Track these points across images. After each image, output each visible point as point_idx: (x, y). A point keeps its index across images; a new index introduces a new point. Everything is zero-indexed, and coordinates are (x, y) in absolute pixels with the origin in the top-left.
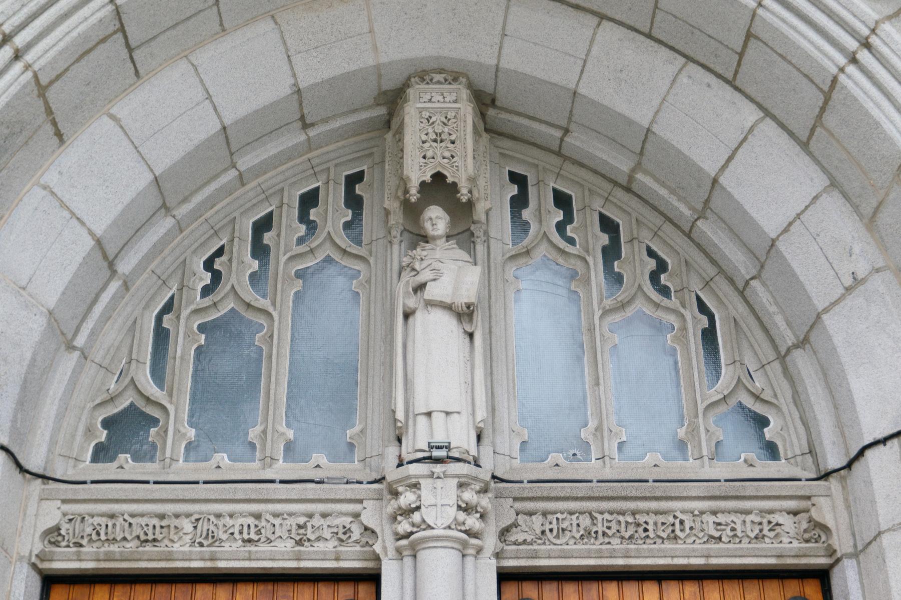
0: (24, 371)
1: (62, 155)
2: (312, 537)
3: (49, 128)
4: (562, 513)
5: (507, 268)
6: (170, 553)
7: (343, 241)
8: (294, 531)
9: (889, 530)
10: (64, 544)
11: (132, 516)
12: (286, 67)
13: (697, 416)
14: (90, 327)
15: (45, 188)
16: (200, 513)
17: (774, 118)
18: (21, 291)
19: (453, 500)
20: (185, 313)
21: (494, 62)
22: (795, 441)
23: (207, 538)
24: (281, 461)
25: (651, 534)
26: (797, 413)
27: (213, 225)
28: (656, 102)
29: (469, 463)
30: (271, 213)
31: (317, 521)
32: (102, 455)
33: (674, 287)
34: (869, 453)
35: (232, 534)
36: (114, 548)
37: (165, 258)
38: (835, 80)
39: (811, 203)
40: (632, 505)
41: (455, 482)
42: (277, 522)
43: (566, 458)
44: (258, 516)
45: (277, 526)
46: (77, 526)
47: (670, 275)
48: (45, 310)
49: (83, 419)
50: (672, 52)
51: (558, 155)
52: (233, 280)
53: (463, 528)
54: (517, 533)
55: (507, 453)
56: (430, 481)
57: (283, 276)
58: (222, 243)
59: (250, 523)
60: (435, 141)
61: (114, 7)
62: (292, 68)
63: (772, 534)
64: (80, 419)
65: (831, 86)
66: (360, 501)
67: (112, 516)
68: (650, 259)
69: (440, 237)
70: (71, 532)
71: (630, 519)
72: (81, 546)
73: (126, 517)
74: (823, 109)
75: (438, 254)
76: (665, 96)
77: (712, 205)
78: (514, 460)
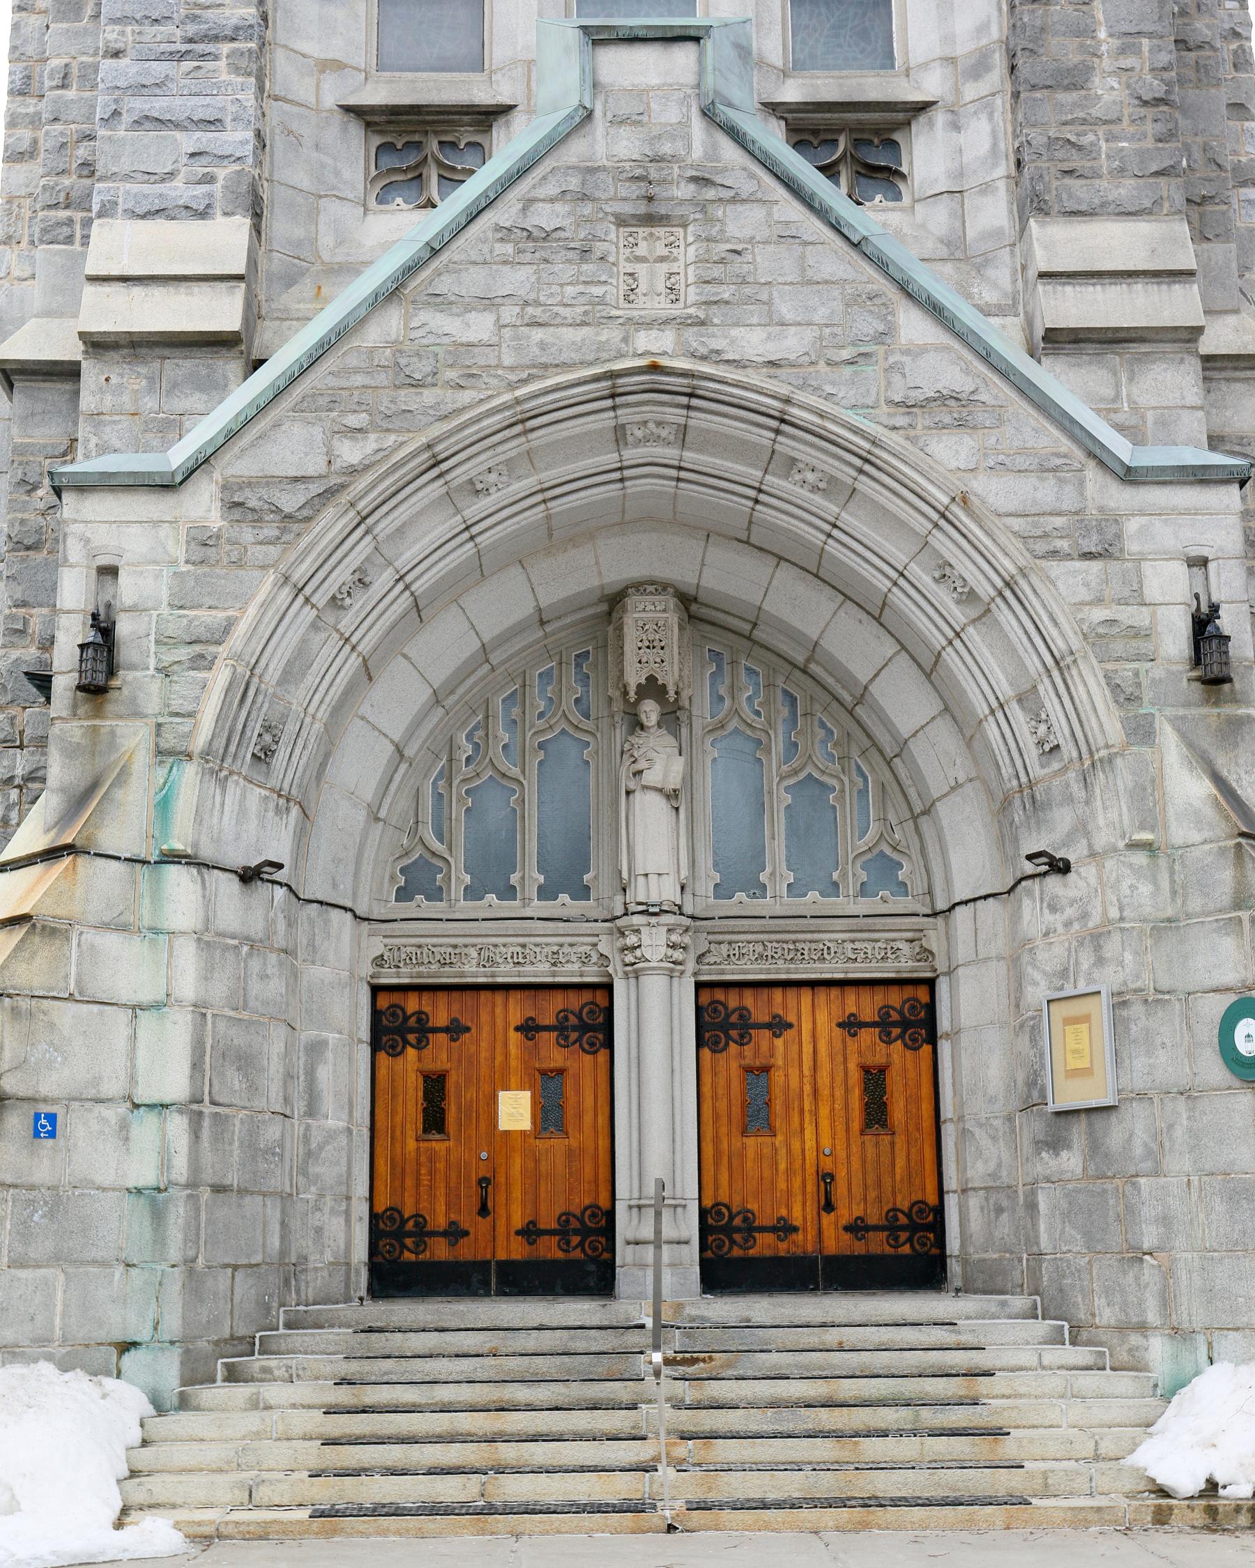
7: (576, 717)
11: (434, 946)
15: (363, 718)
17: (907, 651)
19: (663, 941)
28: (823, 625)
31: (566, 949)
34: (957, 908)
36: (422, 969)
38: (939, 653)
40: (793, 937)
41: (665, 928)
42: (538, 950)
44: (524, 946)
52: (491, 754)
60: (648, 647)
67: (420, 947)
71: (791, 947)
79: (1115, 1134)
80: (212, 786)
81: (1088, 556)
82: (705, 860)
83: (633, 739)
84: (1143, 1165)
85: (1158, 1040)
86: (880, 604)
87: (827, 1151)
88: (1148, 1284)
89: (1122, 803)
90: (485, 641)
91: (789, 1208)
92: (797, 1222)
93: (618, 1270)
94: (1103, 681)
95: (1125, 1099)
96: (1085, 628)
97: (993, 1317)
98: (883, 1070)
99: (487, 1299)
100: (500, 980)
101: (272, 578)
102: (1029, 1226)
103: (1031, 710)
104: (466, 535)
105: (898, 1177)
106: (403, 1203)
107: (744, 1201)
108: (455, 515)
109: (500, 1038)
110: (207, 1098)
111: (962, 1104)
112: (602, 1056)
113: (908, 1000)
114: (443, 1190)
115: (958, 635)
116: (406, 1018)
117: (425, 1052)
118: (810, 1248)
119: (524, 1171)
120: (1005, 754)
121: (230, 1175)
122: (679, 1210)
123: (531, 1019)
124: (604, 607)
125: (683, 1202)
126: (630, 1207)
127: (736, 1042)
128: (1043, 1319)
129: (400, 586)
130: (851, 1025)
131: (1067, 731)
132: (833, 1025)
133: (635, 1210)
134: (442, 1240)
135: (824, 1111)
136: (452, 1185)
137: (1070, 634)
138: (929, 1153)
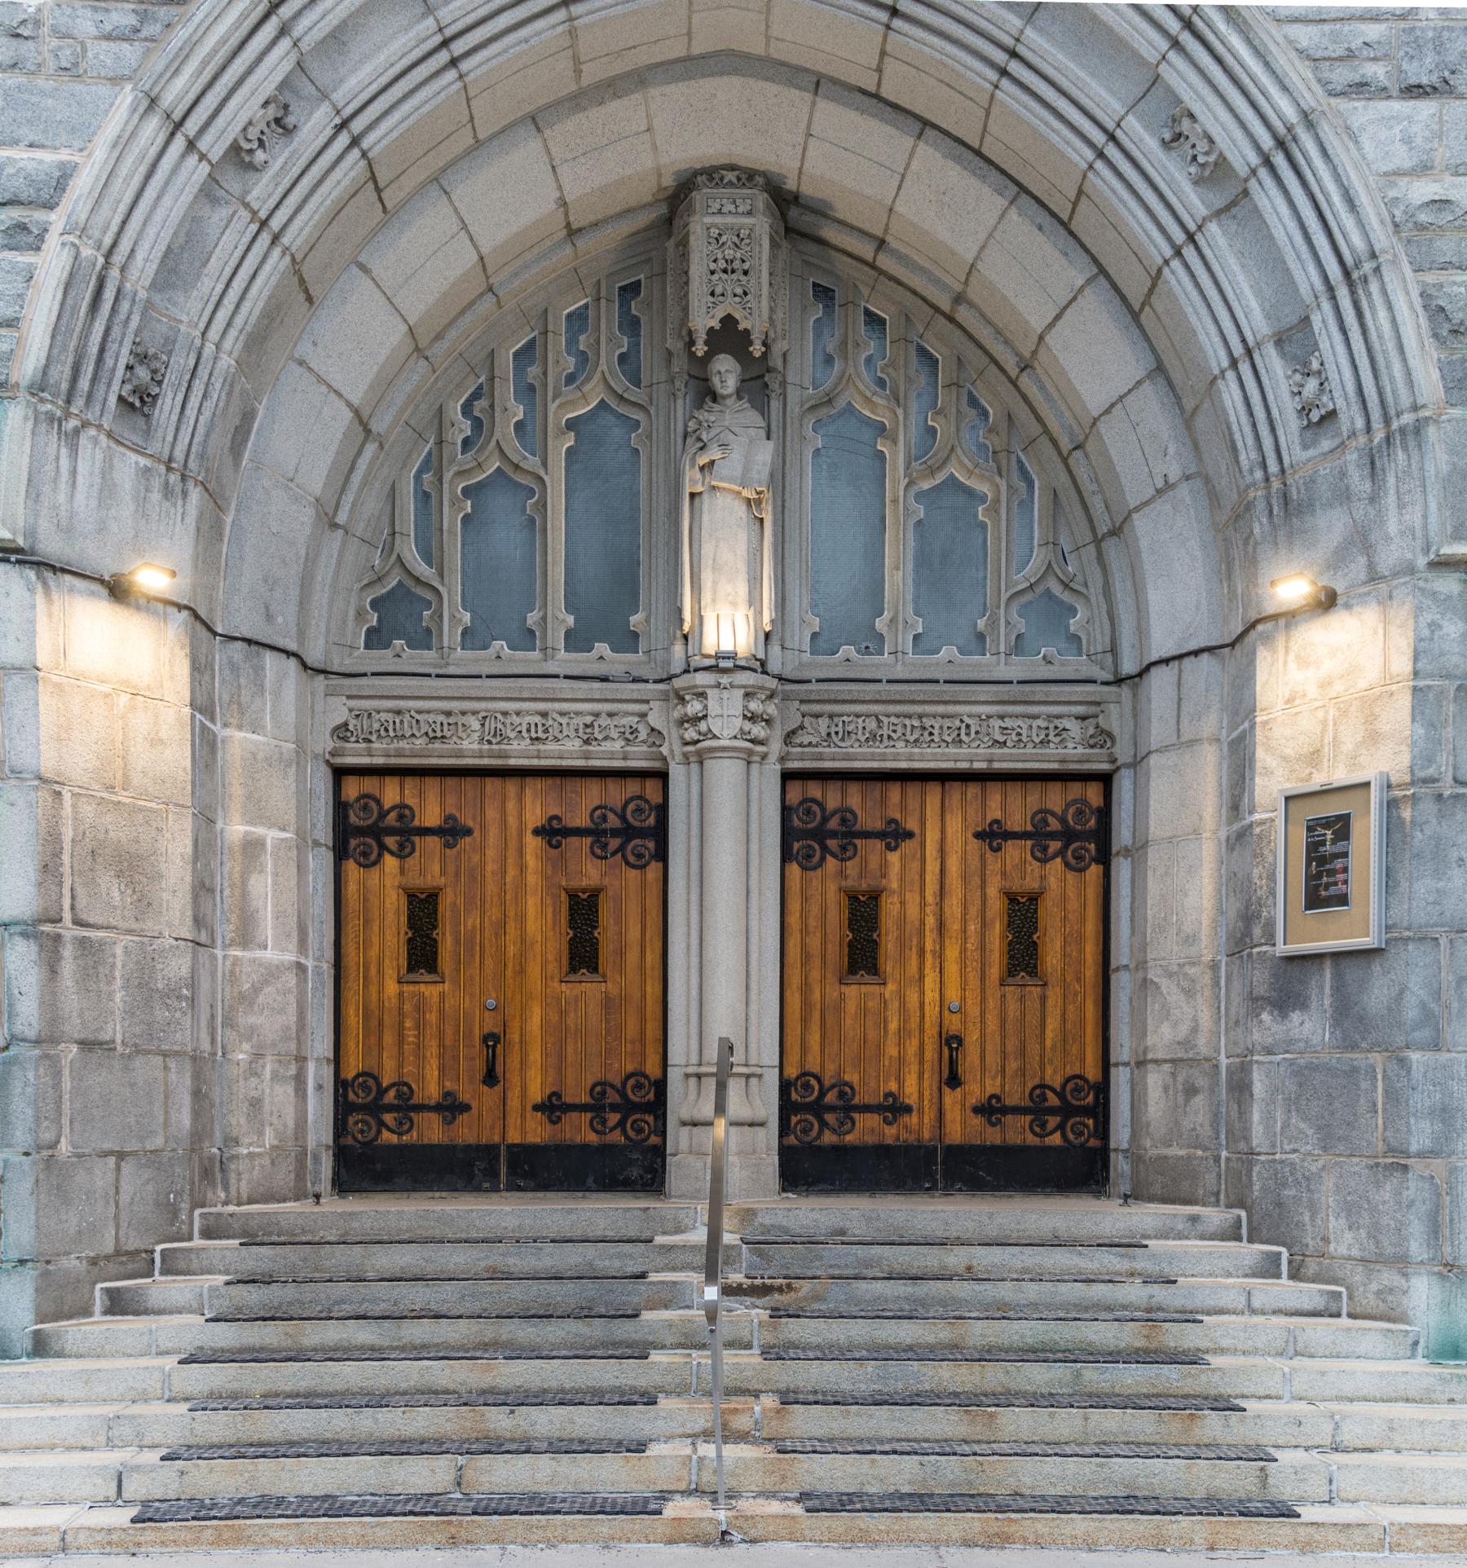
2: (600, 737)
3: (302, 297)
5: (806, 420)
6: (461, 750)
7: (620, 383)
11: (419, 712)
12: (550, 180)
13: (998, 607)
19: (739, 711)
22: (1099, 636)
23: (495, 735)
28: (982, 236)
31: (604, 721)
34: (1154, 671)
36: (403, 744)
38: (1160, 271)
40: (919, 709)
41: (742, 691)
42: (564, 721)
44: (544, 715)
49: (352, 600)
52: (497, 435)
55: (796, 646)
56: (716, 691)
60: (725, 271)
62: (557, 180)
63: (1058, 739)
66: (647, 702)
67: (399, 712)
69: (730, 396)
71: (916, 723)
72: (370, 741)
75: (728, 419)
79: (1377, 993)
80: (51, 442)
81: (1415, 91)
82: (798, 600)
83: (702, 415)
84: (1417, 1034)
85: (1454, 854)
86: (1072, 195)
87: (955, 1005)
88: (1413, 1202)
89: (1430, 498)
91: (900, 1081)
92: (911, 1100)
93: (668, 1159)
94: (1418, 302)
95: (1396, 939)
96: (1397, 213)
97: (1180, 1236)
98: (1034, 898)
99: (495, 1196)
100: (512, 762)
101: (129, 99)
102: (1234, 1114)
103: (1295, 358)
104: (443, 57)
105: (1048, 1043)
106: (380, 1065)
107: (840, 1070)
108: (424, 16)
109: (513, 844)
110: (67, 916)
111: (1144, 948)
112: (653, 871)
113: (1075, 801)
114: (434, 1050)
115: (1191, 238)
117: (412, 862)
118: (927, 1135)
119: (545, 1023)
120: (1247, 429)
121: (110, 1026)
122: (753, 1081)
123: (555, 817)
124: (663, 210)
125: (758, 1071)
126: (687, 1076)
127: (835, 856)
128: (1250, 1241)
129: (343, 140)
130: (993, 836)
131: (1351, 387)
132: (969, 835)
133: (693, 1081)
135: (952, 953)
136: (448, 1042)
137: (1373, 221)
138: (1091, 1012)
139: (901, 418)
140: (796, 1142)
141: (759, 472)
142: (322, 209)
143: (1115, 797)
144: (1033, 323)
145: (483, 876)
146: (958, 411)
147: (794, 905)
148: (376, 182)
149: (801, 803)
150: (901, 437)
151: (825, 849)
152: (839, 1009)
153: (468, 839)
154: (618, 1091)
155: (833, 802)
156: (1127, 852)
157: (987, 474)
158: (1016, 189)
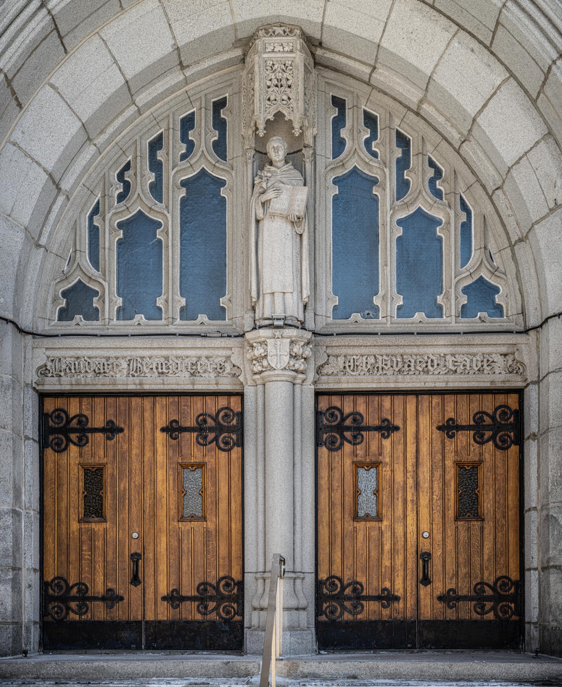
0: (15, 270)
1: (22, 118)
3: (14, 103)
4: (357, 356)
8: (189, 367)
9: (553, 372)
10: (50, 375)
12: (168, 33)
13: (450, 288)
14: (49, 231)
16: (131, 356)
17: (516, 78)
18: (8, 217)
20: (108, 216)
21: (320, 20)
23: (136, 372)
24: (179, 319)
25: (413, 369)
26: (517, 285)
27: (121, 147)
28: (436, 58)
29: (298, 328)
30: (161, 134)
32: (64, 315)
33: (445, 190)
35: (152, 369)
37: (91, 174)
38: (550, 68)
39: (534, 146)
41: (289, 340)
43: (363, 317)
45: (179, 364)
46: (57, 364)
47: (443, 181)
48: (23, 228)
50: (449, 21)
51: (368, 84)
53: (293, 369)
54: (328, 368)
55: (324, 314)
56: (273, 340)
57: (173, 186)
58: (128, 159)
59: (162, 361)
60: (277, 86)
61: (51, 17)
64: (48, 292)
65: (548, 70)
67: (78, 358)
68: (430, 168)
70: (53, 367)
72: (60, 376)
73: (86, 358)
74: (544, 83)
76: (442, 54)
77: (473, 133)
78: (329, 319)
86: (492, 26)
90: (128, 77)
91: (392, 581)
98: (476, 466)
105: (486, 557)
106: (68, 573)
107: (354, 574)
109: (148, 437)
114: (101, 564)
116: (69, 421)
117: (86, 449)
123: (175, 421)
125: (302, 575)
127: (350, 442)
132: (434, 428)
134: (101, 603)
135: (424, 500)
138: (513, 538)
139: (388, 174)
140: (327, 619)
141: (298, 206)
142: (23, 46)
143: (526, 403)
144: (469, 110)
145: (130, 457)
146: (423, 170)
147: (324, 473)
148: (58, 32)
149: (328, 410)
150: (388, 186)
151: (343, 438)
152: (354, 538)
153: (121, 435)
154: (214, 588)
155: (347, 410)
156: (534, 436)
157: (442, 207)
158: (456, 28)
